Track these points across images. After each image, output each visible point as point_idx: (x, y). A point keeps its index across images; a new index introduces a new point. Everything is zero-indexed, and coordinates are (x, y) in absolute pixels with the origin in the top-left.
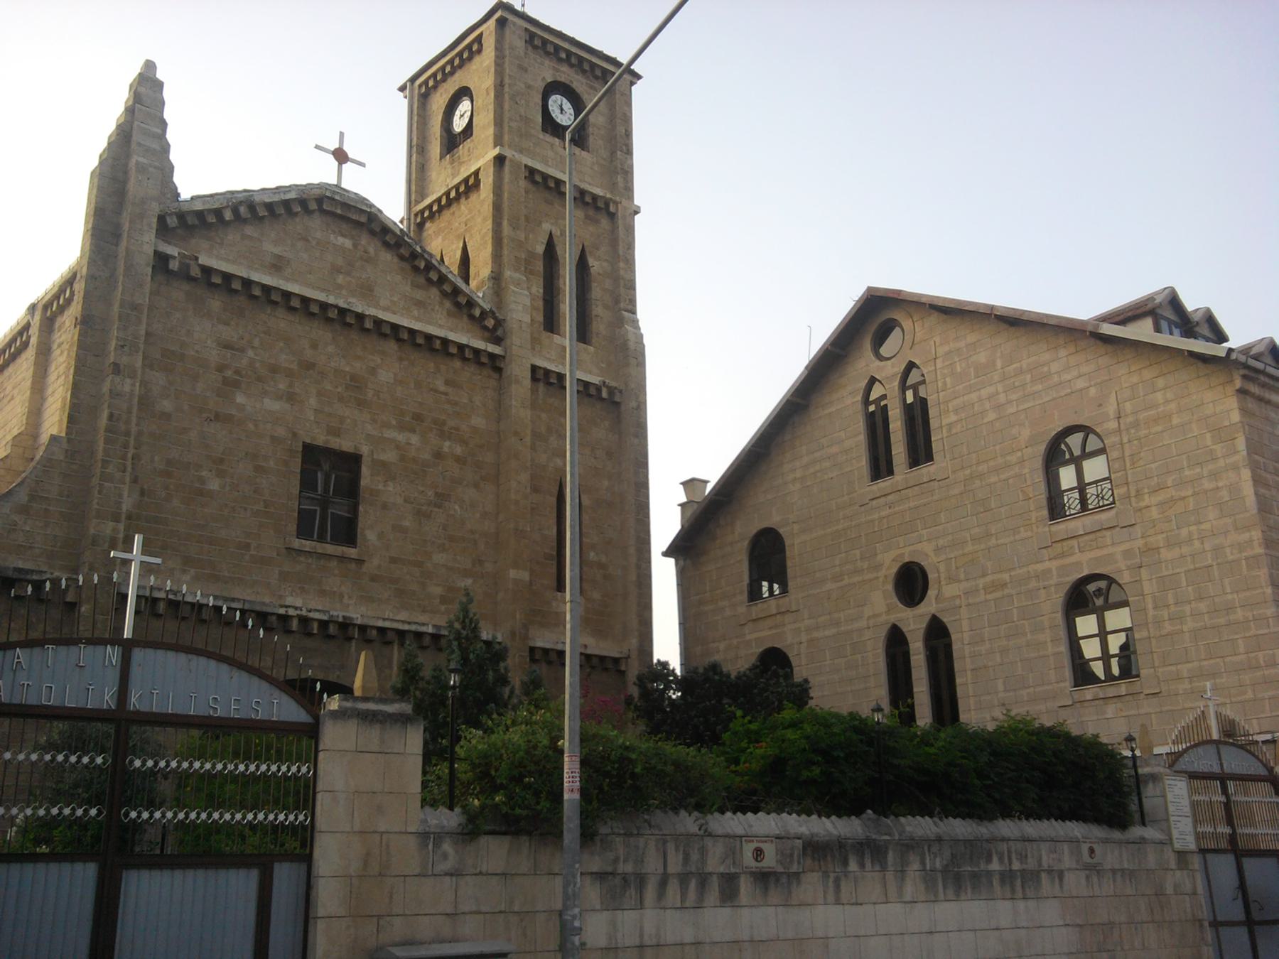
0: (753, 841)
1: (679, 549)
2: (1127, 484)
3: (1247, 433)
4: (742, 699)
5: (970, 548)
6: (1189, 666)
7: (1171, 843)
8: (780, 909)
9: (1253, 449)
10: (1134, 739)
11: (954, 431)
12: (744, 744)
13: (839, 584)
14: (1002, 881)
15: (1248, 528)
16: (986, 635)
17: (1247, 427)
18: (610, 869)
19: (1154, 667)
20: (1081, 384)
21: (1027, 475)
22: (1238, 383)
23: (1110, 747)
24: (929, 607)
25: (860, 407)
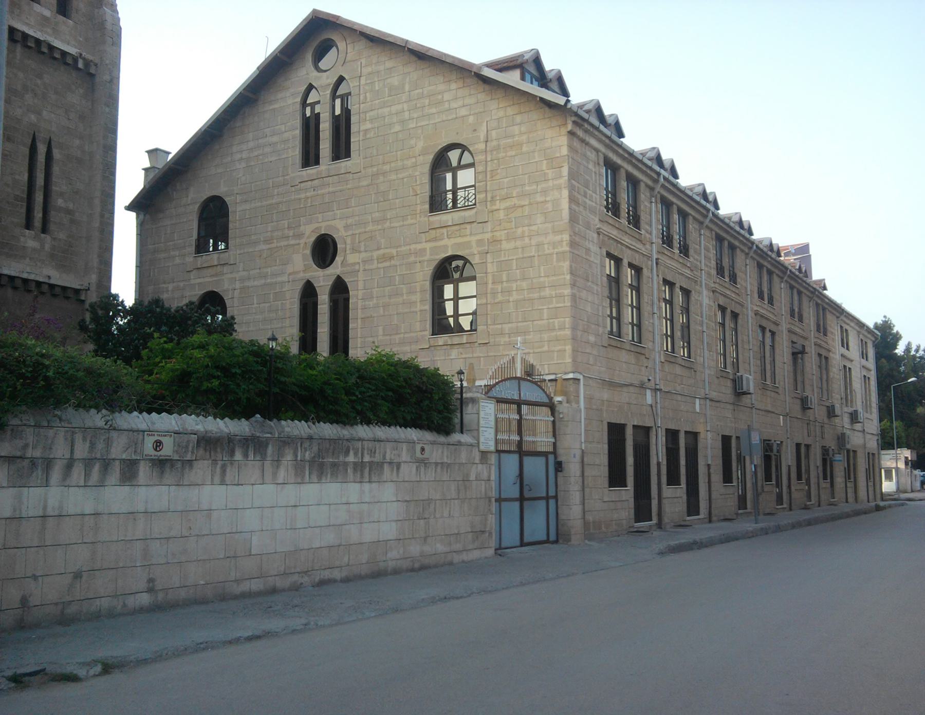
0: (154, 435)
1: (138, 205)
2: (486, 191)
3: (570, 164)
4: (177, 328)
5: (370, 227)
6: (510, 325)
7: (478, 446)
8: (173, 488)
9: (572, 175)
10: (463, 373)
11: (368, 136)
12: (157, 360)
13: (268, 246)
14: (355, 470)
15: (561, 232)
16: (375, 293)
17: (570, 159)
18: (19, 454)
19: (487, 325)
20: (463, 112)
21: (418, 177)
22: (570, 127)
23: (446, 378)
24: (335, 269)
25: (298, 107)
